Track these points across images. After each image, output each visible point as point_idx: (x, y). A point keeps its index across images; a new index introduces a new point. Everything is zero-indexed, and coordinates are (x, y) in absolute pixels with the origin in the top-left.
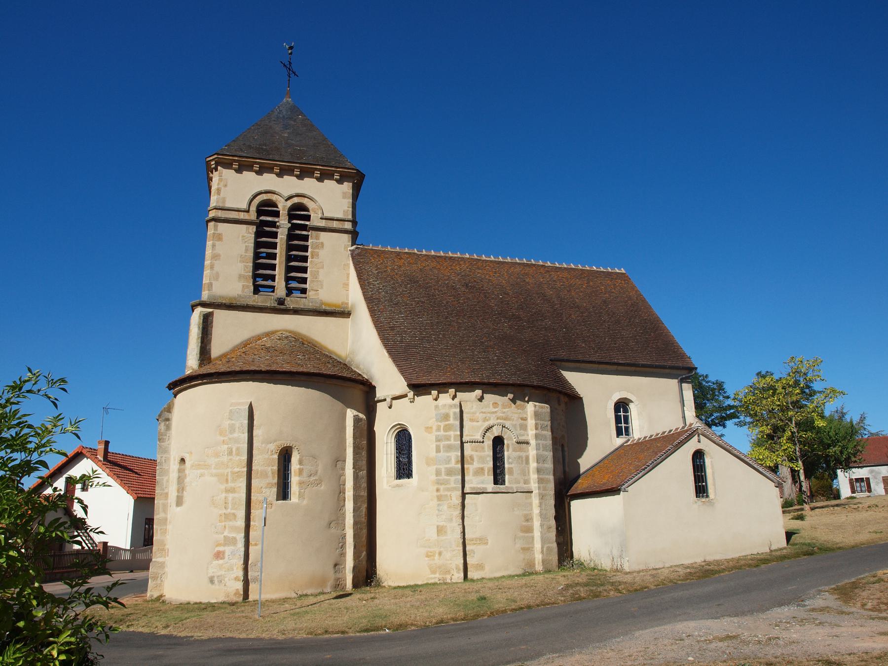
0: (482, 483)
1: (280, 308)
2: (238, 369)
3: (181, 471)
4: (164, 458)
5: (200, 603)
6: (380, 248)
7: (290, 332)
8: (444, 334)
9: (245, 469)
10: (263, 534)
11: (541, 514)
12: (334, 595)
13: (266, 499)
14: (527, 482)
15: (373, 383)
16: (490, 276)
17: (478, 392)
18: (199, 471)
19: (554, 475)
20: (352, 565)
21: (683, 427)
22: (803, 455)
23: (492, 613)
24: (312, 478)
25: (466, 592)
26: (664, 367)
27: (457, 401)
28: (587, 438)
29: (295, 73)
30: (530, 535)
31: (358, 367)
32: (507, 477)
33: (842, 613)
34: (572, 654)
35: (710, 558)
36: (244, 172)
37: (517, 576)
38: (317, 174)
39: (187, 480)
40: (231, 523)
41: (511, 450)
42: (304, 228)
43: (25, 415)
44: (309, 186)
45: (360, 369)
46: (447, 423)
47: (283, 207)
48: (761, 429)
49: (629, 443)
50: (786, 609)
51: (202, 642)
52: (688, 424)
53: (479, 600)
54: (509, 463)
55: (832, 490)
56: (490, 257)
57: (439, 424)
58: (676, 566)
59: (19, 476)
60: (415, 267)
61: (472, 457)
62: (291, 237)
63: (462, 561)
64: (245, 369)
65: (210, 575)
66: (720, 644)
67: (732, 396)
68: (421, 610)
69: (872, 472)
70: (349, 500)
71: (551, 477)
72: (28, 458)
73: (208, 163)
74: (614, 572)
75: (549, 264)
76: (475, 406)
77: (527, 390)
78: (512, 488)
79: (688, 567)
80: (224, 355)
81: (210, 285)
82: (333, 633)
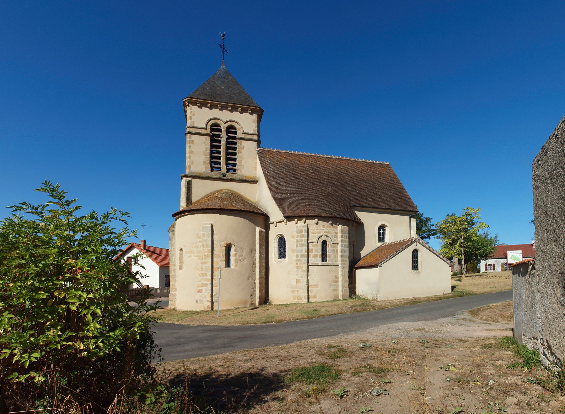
0: (317, 261)
1: (224, 179)
2: (205, 208)
4: (172, 249)
9: (210, 254)
11: (342, 275)
12: (251, 308)
13: (220, 267)
14: (336, 261)
15: (268, 215)
17: (316, 220)
18: (189, 255)
19: (349, 258)
21: (410, 239)
22: (465, 253)
23: (319, 316)
24: (241, 258)
26: (403, 210)
27: (306, 224)
28: (365, 242)
30: (337, 284)
31: (261, 207)
33: (471, 321)
35: (416, 296)
37: (331, 301)
39: (184, 258)
40: (204, 277)
41: (330, 246)
43: (113, 229)
44: (236, 116)
46: (301, 234)
47: (223, 127)
48: (447, 240)
51: (194, 327)
52: (412, 237)
54: (329, 253)
59: (111, 257)
62: (228, 143)
64: (208, 208)
66: (416, 332)
67: (435, 225)
71: (348, 259)
72: (114, 249)
76: (314, 227)
77: (338, 220)
79: (406, 300)
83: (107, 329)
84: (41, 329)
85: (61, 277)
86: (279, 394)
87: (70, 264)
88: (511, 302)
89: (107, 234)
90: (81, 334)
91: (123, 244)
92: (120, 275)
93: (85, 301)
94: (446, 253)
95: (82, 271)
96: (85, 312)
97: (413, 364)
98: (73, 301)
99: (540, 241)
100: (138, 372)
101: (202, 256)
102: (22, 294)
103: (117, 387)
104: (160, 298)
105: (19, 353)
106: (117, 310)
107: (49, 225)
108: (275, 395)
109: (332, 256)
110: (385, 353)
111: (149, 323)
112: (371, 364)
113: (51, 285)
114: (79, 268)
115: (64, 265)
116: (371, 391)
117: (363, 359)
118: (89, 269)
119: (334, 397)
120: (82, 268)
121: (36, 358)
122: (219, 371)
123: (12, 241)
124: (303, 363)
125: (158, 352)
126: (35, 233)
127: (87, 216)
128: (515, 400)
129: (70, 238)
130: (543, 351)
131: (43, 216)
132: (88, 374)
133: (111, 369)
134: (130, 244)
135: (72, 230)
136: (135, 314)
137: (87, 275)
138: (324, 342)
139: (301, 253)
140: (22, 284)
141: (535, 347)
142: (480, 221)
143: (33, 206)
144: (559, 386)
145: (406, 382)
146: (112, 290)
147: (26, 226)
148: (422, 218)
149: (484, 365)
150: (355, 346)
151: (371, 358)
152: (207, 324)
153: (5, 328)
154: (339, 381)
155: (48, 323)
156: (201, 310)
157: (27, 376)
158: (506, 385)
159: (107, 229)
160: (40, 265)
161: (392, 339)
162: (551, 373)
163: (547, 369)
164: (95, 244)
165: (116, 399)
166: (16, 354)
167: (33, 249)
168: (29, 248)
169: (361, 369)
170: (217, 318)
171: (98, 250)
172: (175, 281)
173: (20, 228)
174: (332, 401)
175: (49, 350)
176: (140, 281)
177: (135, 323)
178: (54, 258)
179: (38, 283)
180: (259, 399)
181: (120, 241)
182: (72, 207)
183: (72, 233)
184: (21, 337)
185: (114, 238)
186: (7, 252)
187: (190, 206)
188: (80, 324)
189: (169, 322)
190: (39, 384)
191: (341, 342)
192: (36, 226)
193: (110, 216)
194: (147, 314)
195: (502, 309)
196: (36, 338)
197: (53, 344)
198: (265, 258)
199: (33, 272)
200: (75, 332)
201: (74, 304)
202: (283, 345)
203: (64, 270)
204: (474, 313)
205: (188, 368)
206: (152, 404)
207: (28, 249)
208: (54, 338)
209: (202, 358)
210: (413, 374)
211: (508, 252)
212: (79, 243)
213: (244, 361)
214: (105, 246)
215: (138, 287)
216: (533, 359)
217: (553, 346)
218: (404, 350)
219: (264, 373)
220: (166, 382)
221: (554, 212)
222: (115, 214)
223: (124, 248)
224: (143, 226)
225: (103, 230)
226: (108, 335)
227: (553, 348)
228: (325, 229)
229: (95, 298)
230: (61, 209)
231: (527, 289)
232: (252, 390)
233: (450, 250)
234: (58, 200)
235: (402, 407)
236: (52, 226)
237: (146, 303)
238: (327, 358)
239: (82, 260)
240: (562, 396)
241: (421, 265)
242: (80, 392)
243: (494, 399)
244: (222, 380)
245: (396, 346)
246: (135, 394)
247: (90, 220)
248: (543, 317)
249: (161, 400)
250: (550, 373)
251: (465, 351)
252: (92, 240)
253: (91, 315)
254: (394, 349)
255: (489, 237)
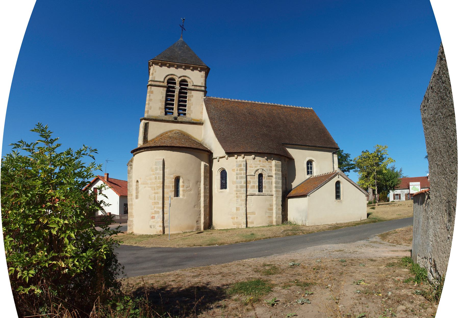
0: (254, 191)
1: (175, 121)
2: (158, 145)
3: (137, 185)
5: (147, 235)
6: (215, 98)
7: (179, 131)
8: (240, 133)
9: (162, 185)
10: (169, 210)
11: (276, 204)
12: (197, 232)
13: (170, 196)
14: (271, 191)
15: (212, 152)
16: (259, 110)
17: (253, 156)
19: (282, 189)
20: (203, 222)
21: (333, 172)
22: (378, 184)
23: (256, 239)
24: (188, 189)
25: (246, 232)
26: (327, 148)
27: (245, 159)
28: (296, 175)
29: (184, 29)
30: (272, 211)
31: (206, 145)
32: (263, 189)
33: (381, 243)
34: (284, 254)
35: (338, 222)
36: (163, 67)
37: (266, 226)
38: (191, 68)
39: (139, 189)
41: (265, 179)
42: (186, 89)
43: (83, 163)
44: (188, 73)
45: (207, 146)
46: (241, 168)
47: (177, 80)
48: (363, 173)
49: (312, 177)
50: (362, 241)
51: (149, 248)
52: (335, 170)
53: (251, 235)
54: (265, 184)
55: (387, 198)
56: (259, 102)
57: (238, 168)
58: (325, 225)
59: (81, 188)
60: (229, 106)
61: (250, 182)
62: (180, 92)
63: (246, 221)
64: (161, 145)
65: (150, 225)
66: (337, 253)
67: (353, 160)
68: (229, 238)
69: (402, 192)
70: (202, 197)
71: (281, 190)
72: (84, 181)
73: (149, 63)
74: (302, 226)
75: (282, 105)
76: (252, 161)
77: (272, 156)
78: (265, 194)
79: (330, 225)
80: (153, 140)
81: (148, 111)
82: (197, 246)
83: (80, 250)
84: (32, 251)
85: (44, 206)
86: (222, 303)
87: (50, 194)
88: (412, 227)
89: (79, 168)
90: (62, 254)
91: (91, 177)
92: (88, 204)
93: (62, 226)
94: (363, 184)
95: (59, 200)
96: (63, 236)
97: (332, 279)
98: (53, 226)
99: (433, 173)
100: (108, 286)
101: (155, 187)
102: (17, 220)
103: (94, 297)
104: (121, 223)
105: (20, 270)
106: (87, 234)
107: (37, 160)
108: (219, 304)
109: (267, 187)
110: (311, 270)
111: (112, 245)
112: (298, 279)
113: (37, 213)
114: (57, 198)
115: (46, 195)
116: (296, 300)
117: (292, 275)
118: (64, 198)
119: (267, 305)
120: (59, 197)
121: (32, 274)
122: (172, 285)
123: (10, 174)
124: (242, 278)
125: (122, 270)
126: (26, 167)
127: (65, 152)
128: (403, 307)
129: (51, 171)
130: (430, 268)
131: (33, 152)
132: (71, 287)
133: (87, 283)
134: (96, 176)
135: (53, 164)
136: (101, 237)
137: (63, 203)
138: (260, 261)
139: (240, 185)
140: (17, 212)
141: (425, 266)
142: (388, 156)
143: (27, 144)
144: (436, 296)
145: (325, 293)
146: (82, 217)
147: (21, 161)
148: (342, 154)
149: (387, 280)
150: (286, 265)
151: (299, 274)
152: (159, 246)
153: (8, 250)
154: (271, 293)
155: (37, 245)
156: (154, 234)
157: (29, 289)
158: (400, 296)
159: (79, 164)
160: (29, 195)
161: (317, 259)
162: (433, 286)
163: (430, 284)
164: (70, 176)
165: (94, 307)
166: (19, 271)
167: (24, 181)
168: (22, 180)
169: (290, 283)
170: (168, 241)
171: (72, 181)
172: (132, 209)
173: (17, 163)
174: (264, 308)
175: (40, 268)
176: (104, 209)
177: (102, 245)
178: (39, 189)
179: (28, 211)
180: (205, 307)
181: (89, 174)
182: (54, 145)
183: (52, 167)
184: (20, 258)
185: (84, 171)
186: (6, 184)
187: (146, 144)
188: (59, 246)
189: (129, 244)
190: (38, 295)
191: (274, 261)
192: (27, 161)
193: (82, 152)
194: (111, 237)
195: (404, 234)
196: (30, 258)
197: (42, 263)
198: (208, 189)
199: (24, 201)
200: (57, 253)
201: (54, 229)
202: (225, 264)
203: (46, 199)
204: (383, 237)
205: (146, 283)
206: (122, 310)
207: (21, 181)
208: (42, 258)
209: (157, 275)
210: (332, 287)
211: (410, 183)
212: (58, 176)
213: (192, 277)
214: (77, 179)
215: (102, 214)
216: (422, 275)
217: (437, 264)
218: (326, 268)
219: (209, 287)
220: (130, 294)
221: (440, 149)
222: (86, 151)
223: (91, 180)
224: (107, 161)
225: (76, 164)
226: (82, 255)
227: (437, 266)
228: (261, 164)
229: (70, 224)
230: (47, 147)
231: (424, 216)
232: (200, 300)
233: (366, 181)
234: (45, 139)
235: (320, 313)
236: (39, 161)
237: (109, 228)
238: (262, 274)
239: (59, 191)
240: (436, 304)
241: (343, 194)
242: (68, 301)
243: (389, 306)
244: (175, 292)
245: (319, 265)
246: (108, 303)
247: (67, 156)
248: (433, 240)
249: (128, 307)
250: (432, 286)
251: (374, 269)
252: (67, 173)
253: (67, 238)
254: (318, 267)
255: (396, 170)
